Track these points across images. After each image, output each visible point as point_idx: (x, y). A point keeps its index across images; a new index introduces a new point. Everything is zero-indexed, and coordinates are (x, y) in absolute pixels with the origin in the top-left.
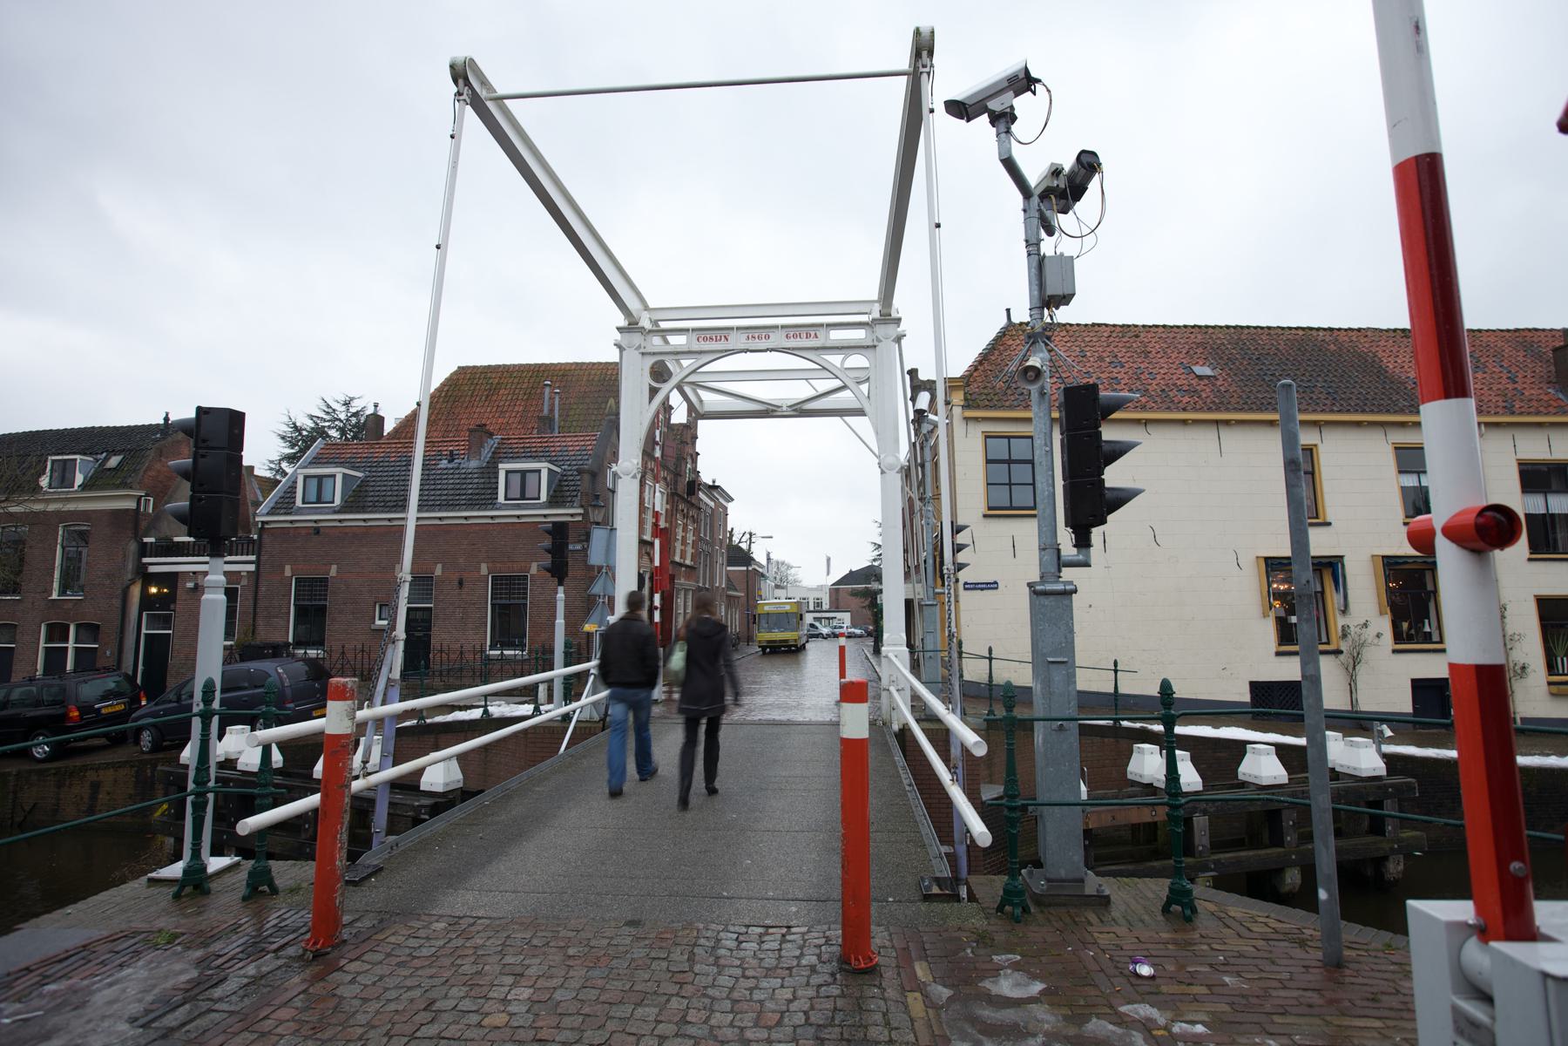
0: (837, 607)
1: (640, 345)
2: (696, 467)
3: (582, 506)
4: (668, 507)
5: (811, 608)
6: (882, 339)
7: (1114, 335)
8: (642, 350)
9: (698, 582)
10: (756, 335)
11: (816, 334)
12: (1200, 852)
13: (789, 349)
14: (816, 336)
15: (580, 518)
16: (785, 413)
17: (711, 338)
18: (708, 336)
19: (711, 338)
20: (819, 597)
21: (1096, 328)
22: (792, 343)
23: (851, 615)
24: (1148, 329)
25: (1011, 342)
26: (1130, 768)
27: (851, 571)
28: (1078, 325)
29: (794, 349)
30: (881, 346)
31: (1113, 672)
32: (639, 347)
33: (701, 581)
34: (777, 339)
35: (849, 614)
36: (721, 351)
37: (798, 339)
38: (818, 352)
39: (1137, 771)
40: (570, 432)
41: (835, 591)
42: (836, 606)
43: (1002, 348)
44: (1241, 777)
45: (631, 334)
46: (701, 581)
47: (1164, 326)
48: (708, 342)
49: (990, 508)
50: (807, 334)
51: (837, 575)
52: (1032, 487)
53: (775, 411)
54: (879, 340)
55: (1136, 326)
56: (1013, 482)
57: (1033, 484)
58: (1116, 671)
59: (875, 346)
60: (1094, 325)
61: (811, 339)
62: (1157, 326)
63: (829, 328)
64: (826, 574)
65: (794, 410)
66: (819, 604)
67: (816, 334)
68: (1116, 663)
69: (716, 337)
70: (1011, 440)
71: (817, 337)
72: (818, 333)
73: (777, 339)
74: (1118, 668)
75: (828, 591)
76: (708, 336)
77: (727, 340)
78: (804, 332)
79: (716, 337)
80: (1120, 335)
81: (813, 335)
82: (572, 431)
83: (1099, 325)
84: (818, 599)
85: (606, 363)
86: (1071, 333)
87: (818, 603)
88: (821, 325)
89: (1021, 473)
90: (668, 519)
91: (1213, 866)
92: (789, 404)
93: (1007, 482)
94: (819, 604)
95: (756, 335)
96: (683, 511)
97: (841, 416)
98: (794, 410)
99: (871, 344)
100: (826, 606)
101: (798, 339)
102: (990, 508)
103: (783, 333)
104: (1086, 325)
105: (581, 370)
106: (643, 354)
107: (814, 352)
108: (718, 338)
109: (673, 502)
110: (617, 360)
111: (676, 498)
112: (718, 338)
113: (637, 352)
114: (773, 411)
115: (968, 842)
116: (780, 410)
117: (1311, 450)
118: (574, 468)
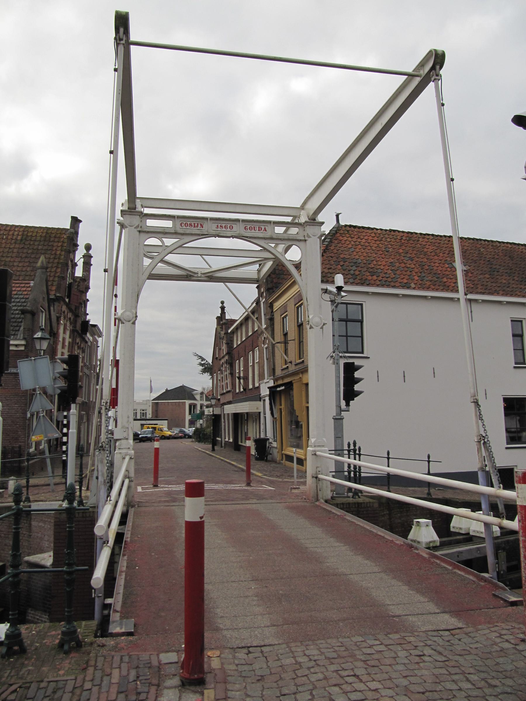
0: (157, 417)
1: (139, 225)
2: (86, 311)
3: (24, 339)
4: (70, 340)
5: (139, 417)
6: (311, 236)
7: (404, 238)
8: (139, 229)
9: (82, 398)
10: (224, 225)
11: (265, 228)
12: (502, 574)
13: (247, 237)
14: (265, 230)
15: (22, 348)
16: (200, 278)
17: (191, 225)
18: (189, 223)
19: (191, 225)
20: (144, 408)
21: (392, 233)
22: (249, 233)
23: (168, 423)
24: (423, 236)
25: (341, 238)
26: (452, 525)
27: (167, 390)
28: (381, 230)
29: (250, 237)
30: (309, 240)
31: (427, 462)
32: (138, 227)
33: (83, 397)
34: (238, 229)
35: (166, 421)
36: (199, 235)
37: (253, 231)
38: (267, 241)
39: (457, 525)
40: (19, 280)
41: (156, 406)
42: (156, 416)
43: (336, 242)
44: (452, 529)
45: (131, 216)
46: (83, 397)
47: (433, 235)
48: (188, 227)
49: (516, 363)
50: (259, 227)
51: (155, 395)
52: (360, 338)
53: (193, 276)
54: (309, 237)
55: (416, 233)
56: (349, 335)
57: (362, 337)
58: (429, 462)
59: (306, 240)
60: (391, 231)
61: (262, 231)
62: (428, 235)
63: (275, 225)
64: (149, 392)
65: (206, 277)
66: (144, 414)
67: (265, 228)
68: (429, 457)
69: (194, 224)
70: (348, 305)
71: (266, 231)
72: (266, 227)
73: (238, 229)
74: (430, 460)
75: (151, 404)
76: (189, 223)
77: (202, 227)
78: (257, 226)
79: (194, 224)
80: (408, 238)
81: (263, 229)
82: (21, 279)
83: (394, 231)
84: (143, 410)
85: (27, 227)
86: (378, 235)
87: (143, 413)
88: (269, 222)
89: (353, 328)
90: (70, 350)
91: (508, 583)
92: (203, 272)
93: (345, 335)
94: (144, 414)
95: (224, 225)
96: (78, 343)
97: (224, 282)
98: (206, 277)
99: (303, 238)
100: (149, 416)
101: (253, 231)
102: (516, 363)
103: (242, 226)
104: (386, 230)
105: (5, 230)
106: (140, 232)
107: (264, 241)
108: (196, 225)
109: (74, 336)
110: (277, 249)
111: (76, 334)
112: (196, 225)
113: (136, 230)
114: (191, 276)
115: (497, 570)
116: (196, 275)
117: (521, 321)
118: (19, 308)
